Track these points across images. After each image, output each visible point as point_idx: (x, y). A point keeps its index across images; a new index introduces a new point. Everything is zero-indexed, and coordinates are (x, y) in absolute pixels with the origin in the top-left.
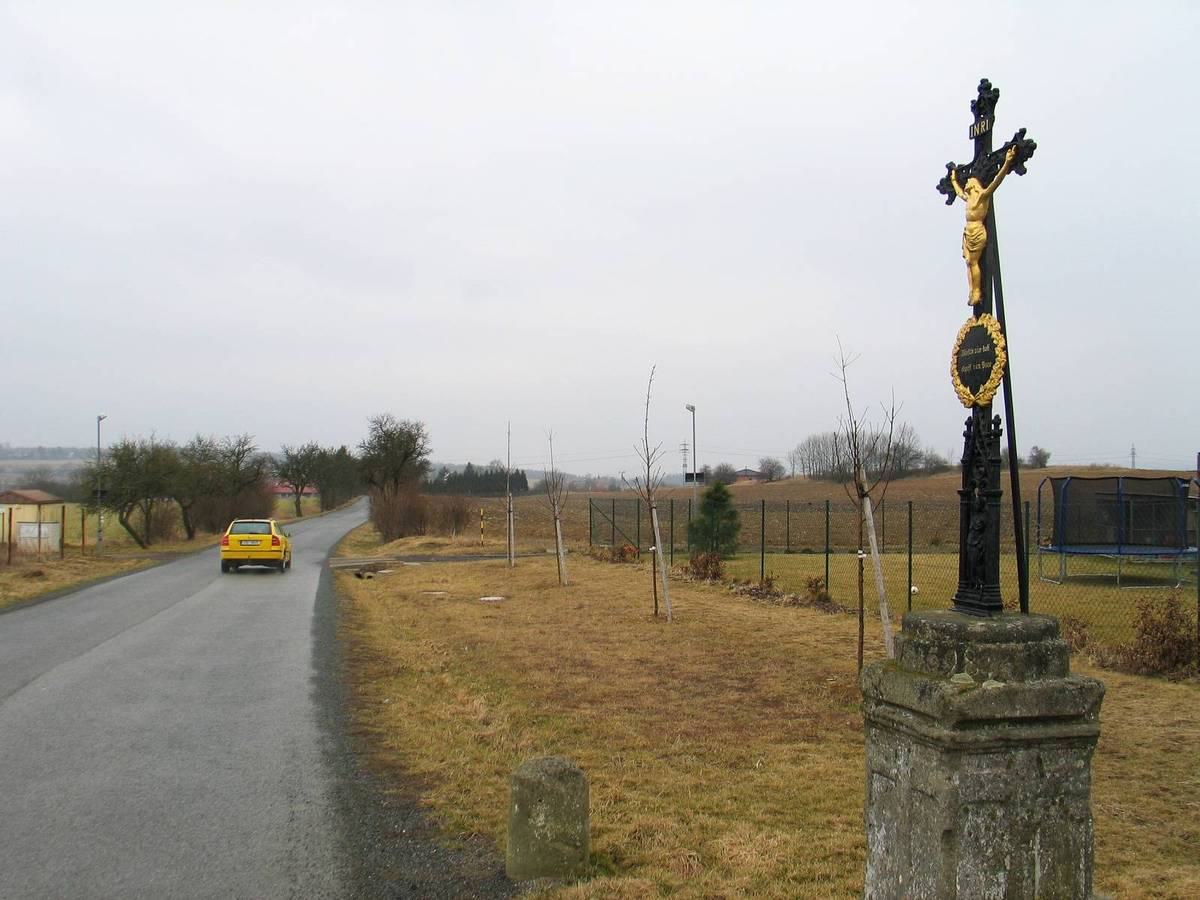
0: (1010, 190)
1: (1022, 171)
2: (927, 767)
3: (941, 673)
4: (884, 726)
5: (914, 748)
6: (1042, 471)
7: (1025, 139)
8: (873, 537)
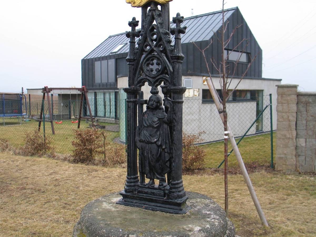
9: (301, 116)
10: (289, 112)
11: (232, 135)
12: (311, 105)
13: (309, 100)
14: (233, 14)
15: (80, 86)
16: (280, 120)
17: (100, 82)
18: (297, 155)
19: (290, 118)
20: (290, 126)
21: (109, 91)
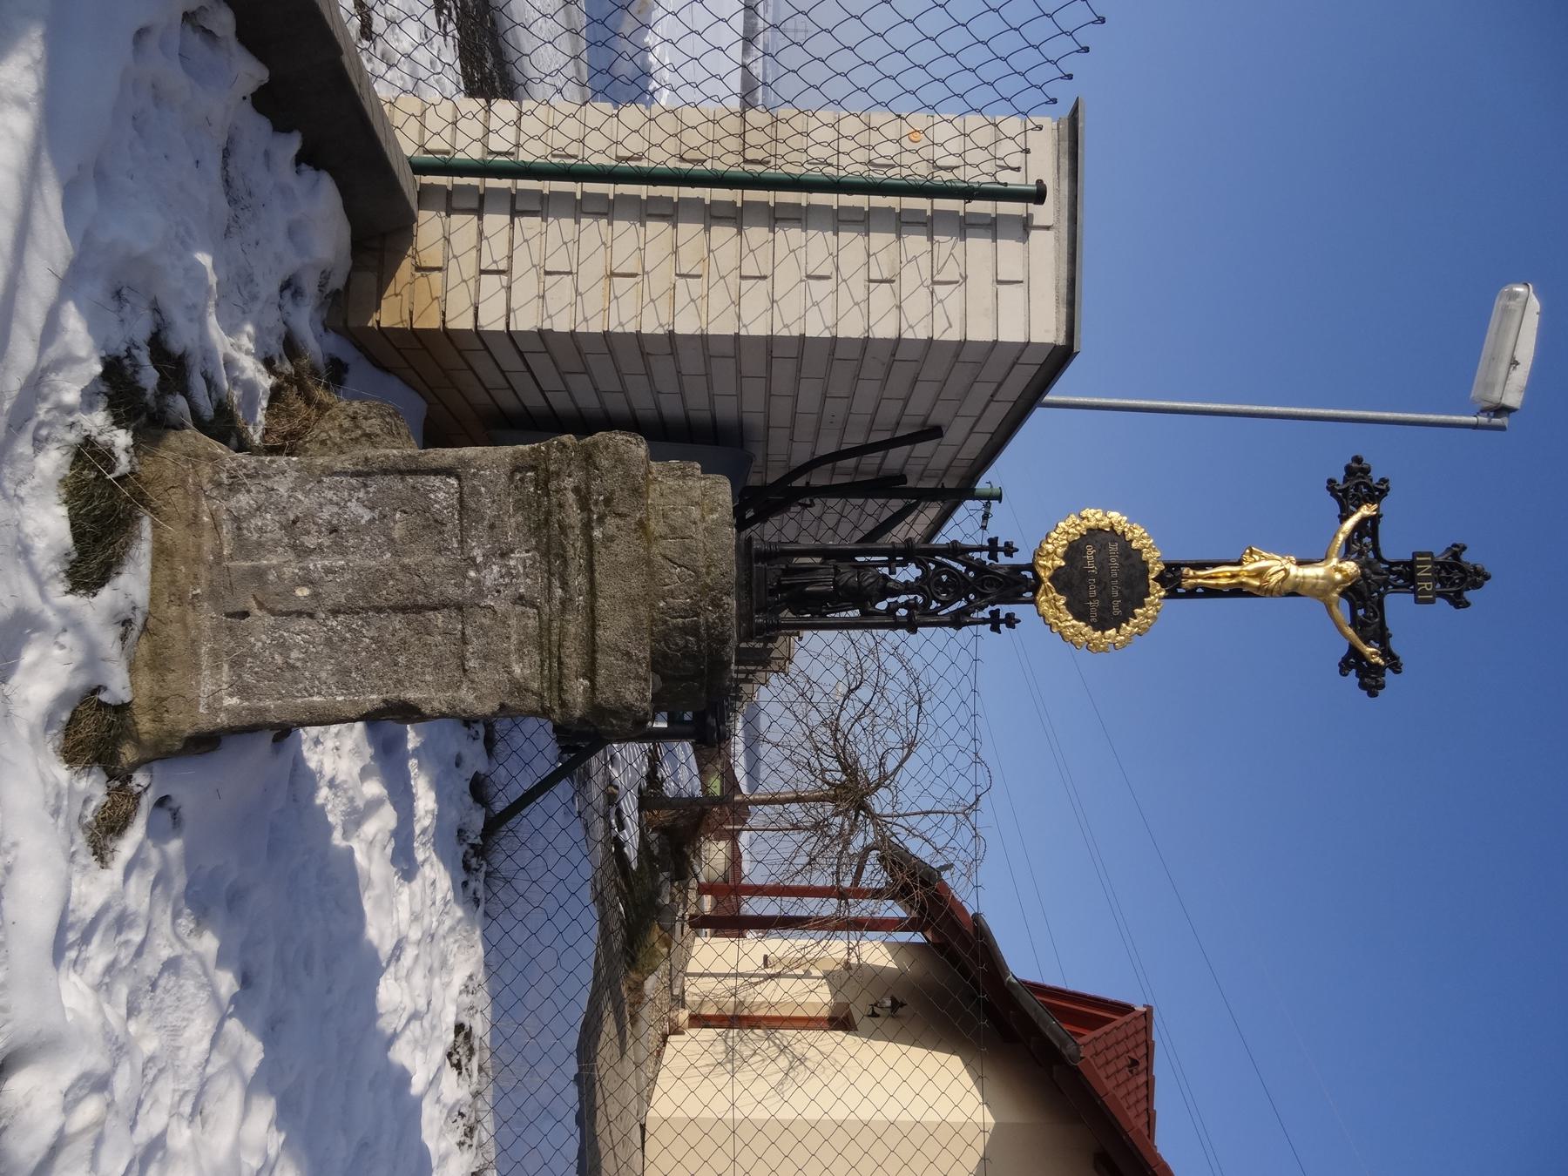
0: (1334, 633)
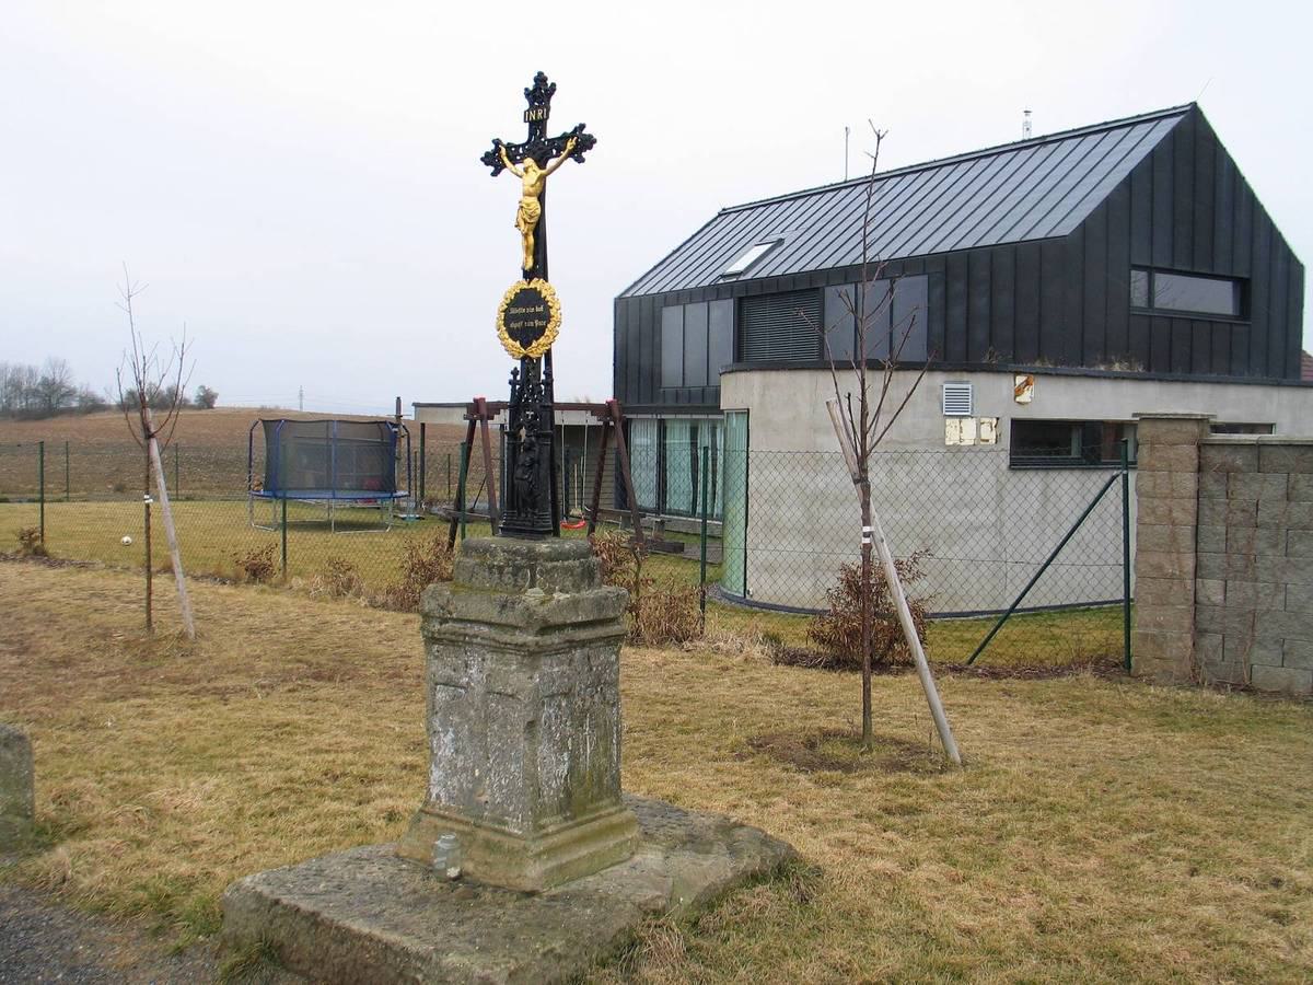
0: (565, 176)
1: (580, 160)
2: (506, 671)
3: (517, 589)
4: (452, 641)
5: (488, 656)
6: (209, 411)
7: (584, 132)
8: (161, 481)
9: (1212, 509)
10: (1173, 498)
11: (880, 534)
12: (1240, 477)
13: (1233, 461)
14: (1174, 135)
15: (610, 397)
16: (1147, 520)
17: (680, 384)
18: (1199, 632)
19: (1174, 515)
20: (1174, 538)
21: (711, 417)
